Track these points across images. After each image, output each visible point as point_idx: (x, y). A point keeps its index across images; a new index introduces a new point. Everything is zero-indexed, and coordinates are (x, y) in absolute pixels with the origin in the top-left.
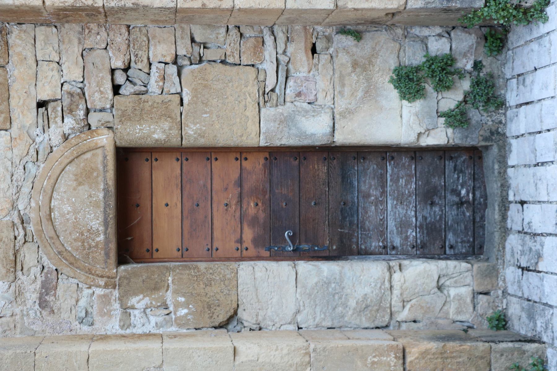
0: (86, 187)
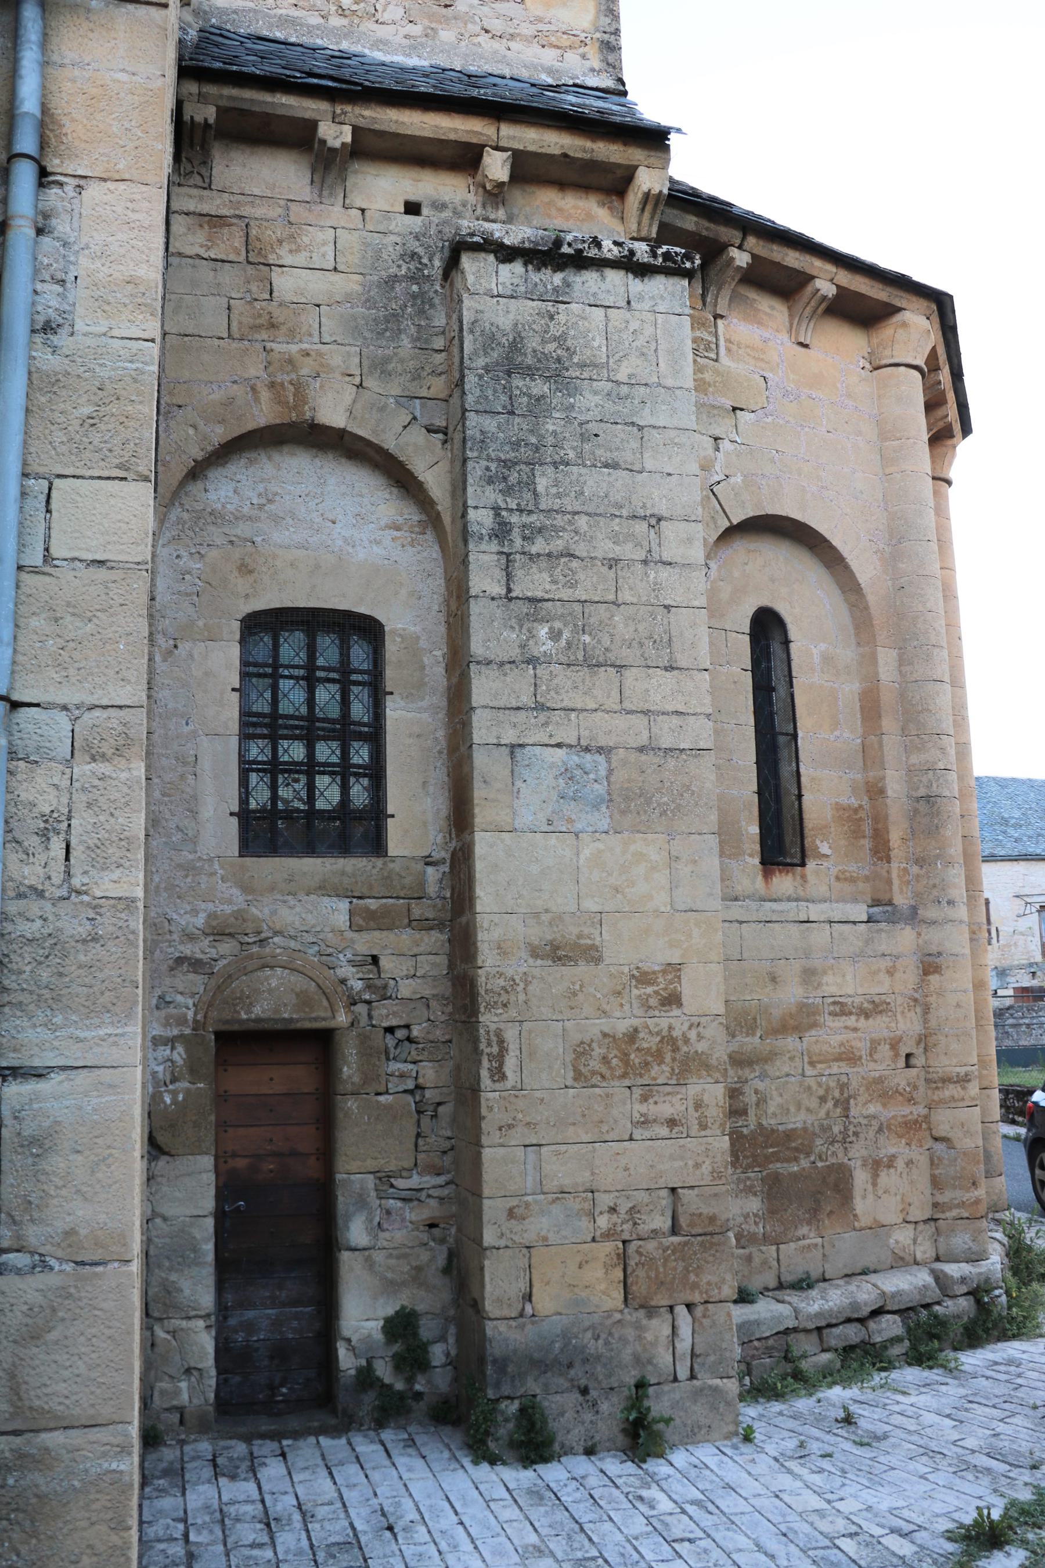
0: (294, 1001)
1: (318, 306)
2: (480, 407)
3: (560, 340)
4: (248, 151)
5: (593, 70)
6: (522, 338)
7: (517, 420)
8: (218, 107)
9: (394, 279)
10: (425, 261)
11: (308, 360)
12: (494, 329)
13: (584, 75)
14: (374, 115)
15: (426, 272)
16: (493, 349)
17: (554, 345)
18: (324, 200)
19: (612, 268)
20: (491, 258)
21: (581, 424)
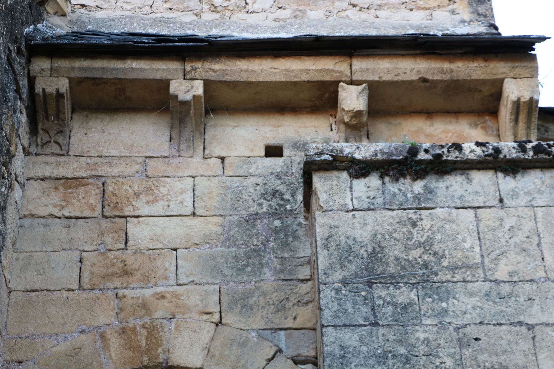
1: (176, 250)
2: (337, 322)
3: (426, 245)
4: (107, 118)
5: (463, 22)
6: (382, 248)
7: (381, 331)
8: (69, 78)
9: (256, 216)
10: (287, 196)
11: (164, 302)
12: (350, 242)
13: (455, 26)
14: (223, 67)
15: (288, 207)
16: (350, 261)
17: (419, 251)
18: (182, 153)
19: (479, 169)
20: (345, 175)
21: (457, 329)
